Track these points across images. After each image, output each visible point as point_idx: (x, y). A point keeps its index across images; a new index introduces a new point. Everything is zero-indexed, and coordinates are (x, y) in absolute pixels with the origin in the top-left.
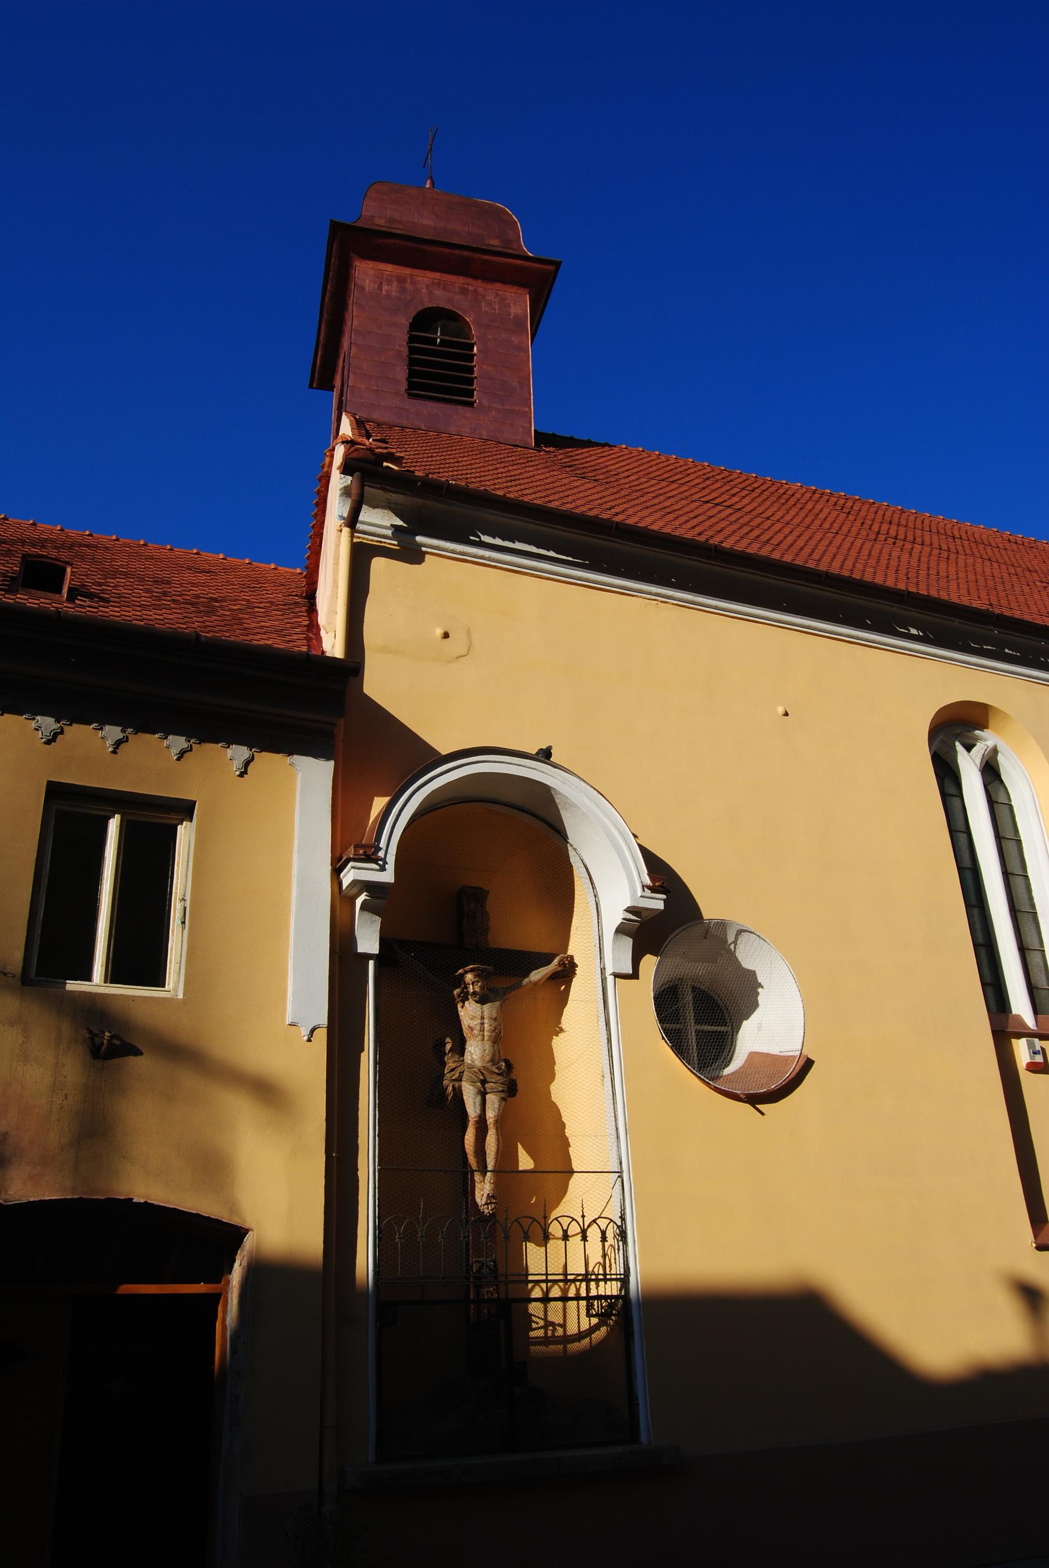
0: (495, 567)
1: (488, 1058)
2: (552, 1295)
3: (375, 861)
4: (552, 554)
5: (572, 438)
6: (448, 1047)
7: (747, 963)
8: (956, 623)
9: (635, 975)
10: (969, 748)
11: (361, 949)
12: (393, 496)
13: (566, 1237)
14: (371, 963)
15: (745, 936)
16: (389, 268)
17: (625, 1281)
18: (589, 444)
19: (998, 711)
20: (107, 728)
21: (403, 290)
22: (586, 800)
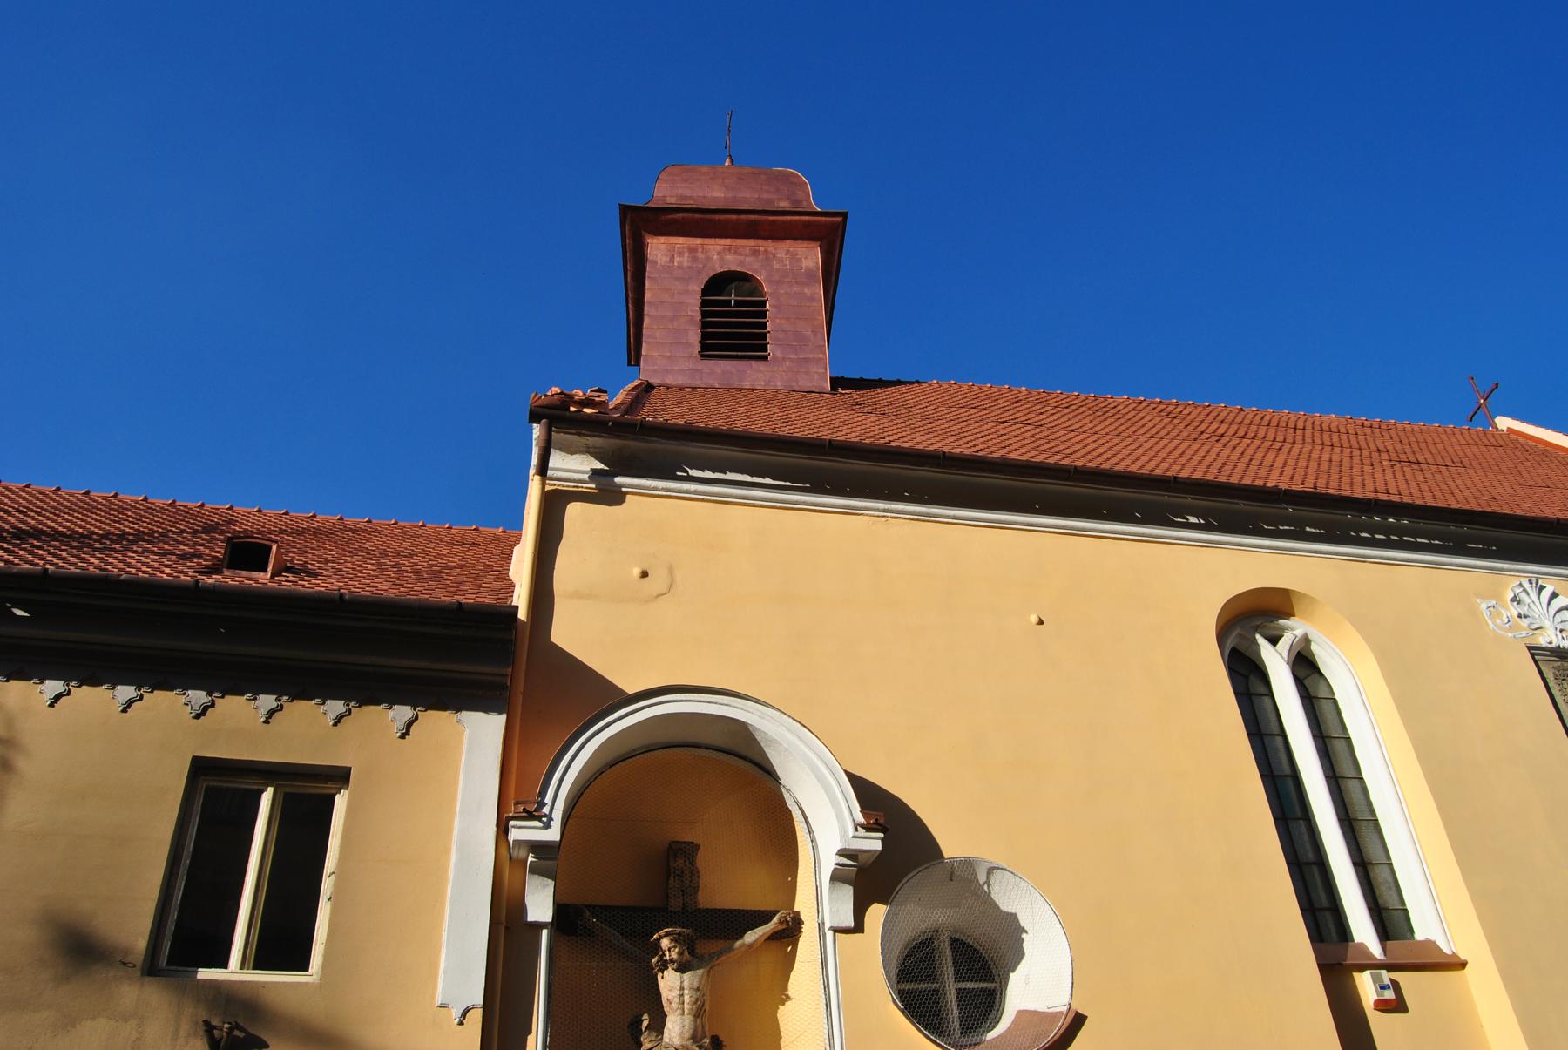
1: (687, 1035)
3: (539, 818)
4: (768, 481)
5: (880, 380)
6: (645, 1024)
7: (1006, 906)
8: (1241, 505)
9: (858, 927)
10: (1274, 641)
11: (531, 918)
12: (591, 441)
14: (545, 932)
15: (997, 875)
16: (680, 241)
18: (899, 383)
19: (1302, 596)
20: (262, 697)
21: (695, 259)
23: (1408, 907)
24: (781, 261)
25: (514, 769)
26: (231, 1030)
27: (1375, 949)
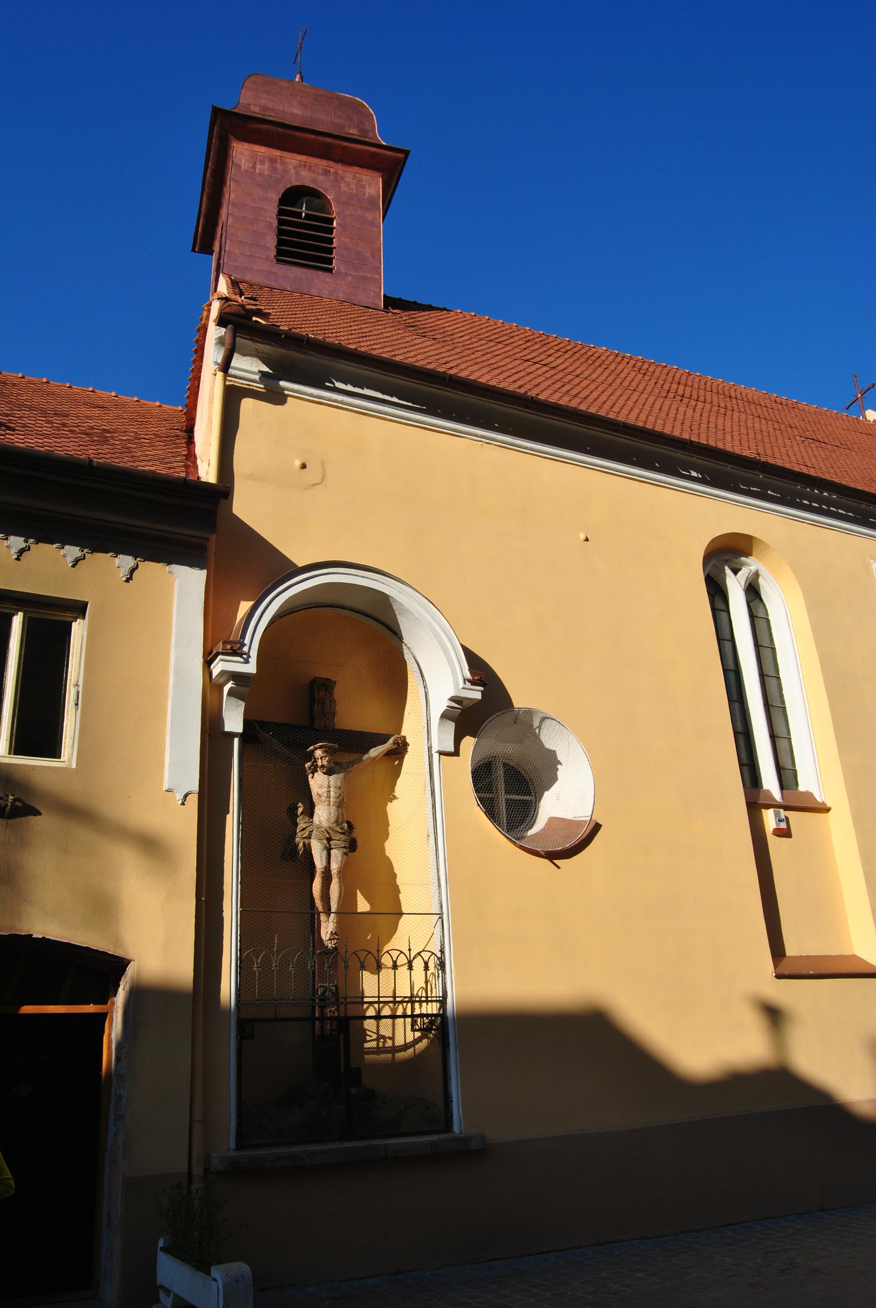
0: (346, 409)
1: (333, 820)
2: (383, 1013)
3: (240, 655)
4: (395, 400)
5: (415, 303)
6: (300, 810)
7: (549, 745)
8: (679, 455)
9: (456, 753)
10: (736, 571)
11: (227, 729)
12: (261, 347)
13: (395, 967)
14: (236, 740)
15: (548, 721)
16: (262, 150)
17: (443, 1002)
18: (430, 308)
20: (12, 538)
21: (274, 169)
22: (418, 607)
23: (797, 768)
24: (348, 184)
25: (211, 614)
26: (15, 800)
27: (777, 795)
